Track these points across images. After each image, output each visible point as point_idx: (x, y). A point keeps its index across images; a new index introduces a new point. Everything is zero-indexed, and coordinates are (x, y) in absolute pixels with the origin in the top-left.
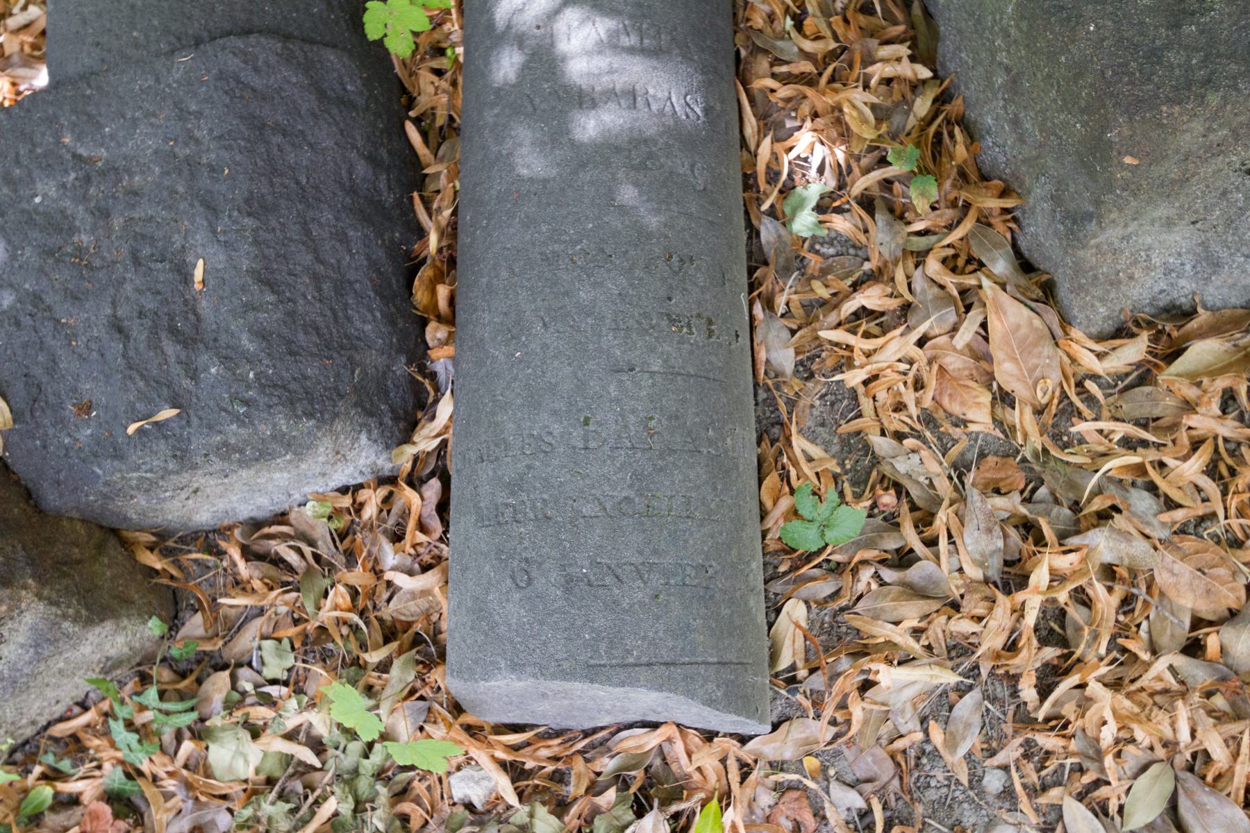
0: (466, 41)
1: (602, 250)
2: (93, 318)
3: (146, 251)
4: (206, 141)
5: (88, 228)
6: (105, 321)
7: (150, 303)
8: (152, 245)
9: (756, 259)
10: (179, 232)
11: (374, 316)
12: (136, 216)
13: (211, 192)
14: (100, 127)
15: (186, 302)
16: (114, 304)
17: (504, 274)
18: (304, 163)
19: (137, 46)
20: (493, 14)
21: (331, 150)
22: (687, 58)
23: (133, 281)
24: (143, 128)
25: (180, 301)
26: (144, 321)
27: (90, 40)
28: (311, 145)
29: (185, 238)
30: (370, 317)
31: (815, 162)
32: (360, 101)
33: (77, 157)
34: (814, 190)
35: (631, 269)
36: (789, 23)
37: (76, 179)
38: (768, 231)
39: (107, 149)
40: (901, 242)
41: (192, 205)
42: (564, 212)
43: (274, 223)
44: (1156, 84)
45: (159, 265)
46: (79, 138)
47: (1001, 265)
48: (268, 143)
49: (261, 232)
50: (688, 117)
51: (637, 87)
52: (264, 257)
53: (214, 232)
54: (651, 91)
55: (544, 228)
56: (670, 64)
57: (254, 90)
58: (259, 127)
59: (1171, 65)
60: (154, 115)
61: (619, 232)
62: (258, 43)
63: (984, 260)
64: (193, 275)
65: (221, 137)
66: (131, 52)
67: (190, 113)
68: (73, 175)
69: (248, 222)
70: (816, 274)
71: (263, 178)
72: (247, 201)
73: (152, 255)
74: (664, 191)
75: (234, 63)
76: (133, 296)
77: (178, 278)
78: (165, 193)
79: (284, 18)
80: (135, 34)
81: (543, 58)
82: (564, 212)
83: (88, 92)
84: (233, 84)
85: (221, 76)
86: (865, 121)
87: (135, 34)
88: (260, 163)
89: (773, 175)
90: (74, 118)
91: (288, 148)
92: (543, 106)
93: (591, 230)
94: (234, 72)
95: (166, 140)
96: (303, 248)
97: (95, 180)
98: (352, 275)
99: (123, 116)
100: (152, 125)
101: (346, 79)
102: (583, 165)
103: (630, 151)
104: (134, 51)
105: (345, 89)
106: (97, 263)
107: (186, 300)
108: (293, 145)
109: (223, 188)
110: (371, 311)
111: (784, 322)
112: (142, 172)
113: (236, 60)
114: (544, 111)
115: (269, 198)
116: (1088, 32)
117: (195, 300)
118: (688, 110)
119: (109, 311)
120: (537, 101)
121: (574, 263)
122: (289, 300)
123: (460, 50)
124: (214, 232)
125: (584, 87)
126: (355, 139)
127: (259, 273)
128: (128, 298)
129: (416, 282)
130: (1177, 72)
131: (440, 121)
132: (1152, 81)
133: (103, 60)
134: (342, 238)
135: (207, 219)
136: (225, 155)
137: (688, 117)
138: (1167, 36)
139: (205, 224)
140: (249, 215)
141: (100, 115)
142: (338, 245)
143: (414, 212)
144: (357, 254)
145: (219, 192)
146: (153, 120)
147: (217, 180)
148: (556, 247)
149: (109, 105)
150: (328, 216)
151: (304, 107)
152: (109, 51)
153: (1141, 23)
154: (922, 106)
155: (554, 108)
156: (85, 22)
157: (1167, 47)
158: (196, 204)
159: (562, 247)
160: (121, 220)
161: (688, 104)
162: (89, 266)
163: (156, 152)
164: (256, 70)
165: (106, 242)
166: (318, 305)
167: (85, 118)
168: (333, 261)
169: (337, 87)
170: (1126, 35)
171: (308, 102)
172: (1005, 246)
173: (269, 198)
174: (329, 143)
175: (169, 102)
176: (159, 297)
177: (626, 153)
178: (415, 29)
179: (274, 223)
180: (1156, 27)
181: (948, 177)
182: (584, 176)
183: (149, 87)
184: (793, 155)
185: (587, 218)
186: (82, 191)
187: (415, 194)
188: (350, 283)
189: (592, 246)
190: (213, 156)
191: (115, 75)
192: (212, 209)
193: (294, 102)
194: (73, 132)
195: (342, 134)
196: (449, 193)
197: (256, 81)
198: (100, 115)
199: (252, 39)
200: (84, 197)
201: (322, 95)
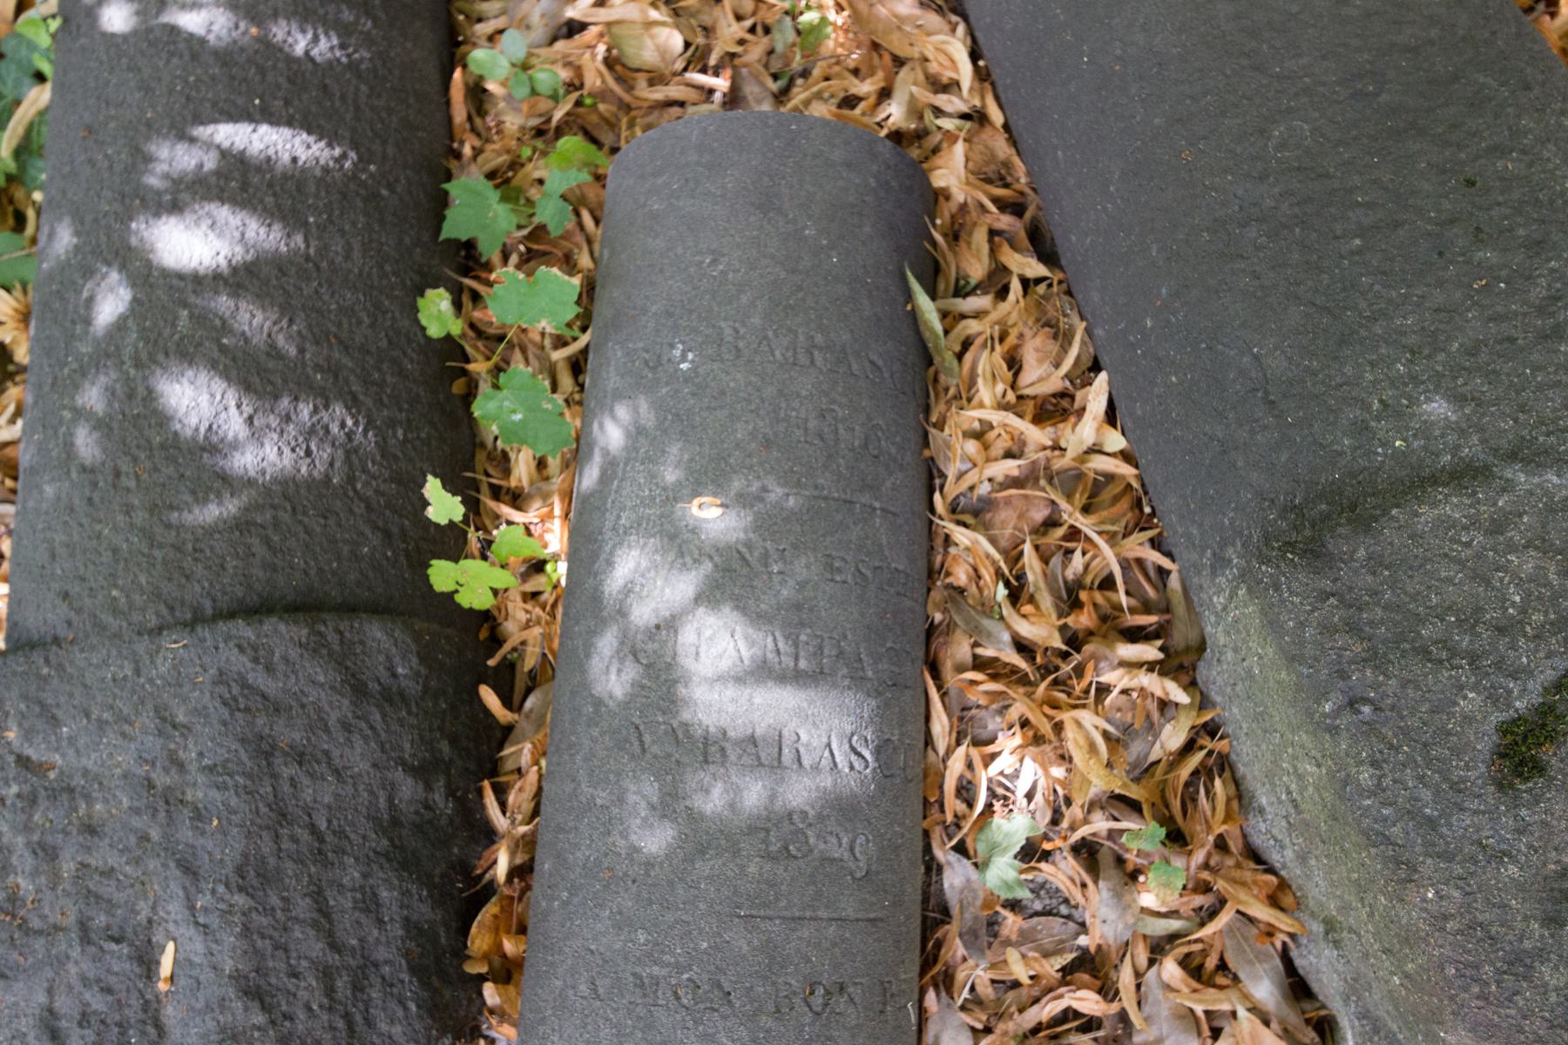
0: (574, 556)
1: (719, 986)
2: (22, 1004)
3: (101, 920)
4: (193, 768)
5: (27, 869)
6: (37, 1012)
7: (98, 1003)
8: (108, 913)
9: (935, 913)
10: (146, 899)
11: (406, 1009)
12: (93, 863)
13: (193, 847)
14: (55, 722)
15: (146, 1006)
16: (50, 992)
17: (584, 988)
18: (326, 800)
19: (115, 611)
20: (601, 583)
21: (364, 774)
22: (857, 680)
23: (79, 962)
24: (111, 737)
25: (135, 1002)
26: (87, 1032)
27: (56, 586)
28: (337, 772)
29: (154, 908)
30: (400, 1013)
31: (1022, 787)
32: (413, 688)
33: (23, 762)
34: (1014, 826)
35: (754, 1015)
36: (1002, 592)
37: (19, 796)
38: (956, 876)
39: (63, 755)
40: (1131, 921)
41: (165, 866)
42: (670, 917)
43: (275, 900)
44: (1520, 1009)
45: (114, 946)
46: (28, 735)
47: (1265, 989)
48: (275, 777)
49: (254, 915)
50: (852, 768)
51: (785, 732)
52: (256, 951)
53: (192, 908)
54: (804, 737)
55: (642, 937)
56: (834, 693)
57: (264, 696)
58: (264, 750)
59: (1545, 985)
60: (127, 721)
61: (744, 957)
62: (276, 630)
63: (1242, 975)
64: (158, 963)
65: (211, 769)
66: (107, 618)
67: (174, 727)
68: (14, 789)
69: (240, 900)
70: (1014, 937)
71: (264, 834)
72: (240, 871)
73: (108, 928)
74: (811, 890)
75: (239, 662)
76: (78, 987)
77: (138, 970)
78: (133, 840)
79: (321, 570)
80: (114, 593)
81: (660, 676)
82: (670, 917)
83: (45, 671)
84: (236, 690)
85: (221, 678)
86: (1092, 748)
87: (114, 593)
88: (264, 810)
89: (966, 791)
90: (22, 706)
91: (306, 781)
92: (655, 749)
93: (705, 952)
94: (239, 673)
95: (141, 759)
96: (312, 933)
97: (43, 803)
98: (381, 954)
99: (87, 716)
100: (124, 735)
101: (397, 659)
102: (702, 851)
103: (768, 831)
104: (111, 619)
105: (394, 675)
106: (35, 923)
107: (147, 1002)
108: (311, 775)
109: (210, 845)
110: (402, 1002)
111: (965, 1018)
112: (106, 801)
113: (244, 659)
114: (655, 757)
115: (272, 861)
116: (1424, 900)
117: (158, 1001)
118: (853, 758)
119: (42, 998)
120: (647, 739)
121: (678, 998)
122: (286, 1016)
123: (563, 567)
124: (192, 908)
125: (712, 729)
126: (403, 750)
127: (246, 978)
128: (70, 987)
129: (474, 930)
130: (1553, 998)
131: (530, 662)
132: (1515, 1004)
133: (69, 623)
134: (369, 904)
135: (185, 888)
136: (215, 794)
137: (852, 768)
138: (1542, 936)
139: (181, 893)
140: (241, 889)
141: (58, 705)
142: (363, 920)
143: (483, 807)
144: (384, 931)
145: (203, 847)
146: (126, 727)
147: (203, 833)
148: (656, 970)
149: (71, 695)
150: (352, 874)
151: (333, 718)
152: (79, 611)
153: (1504, 906)
154: (1173, 736)
155: (669, 756)
156: (53, 556)
157: (1541, 954)
158: (172, 865)
159: (664, 972)
160: (72, 866)
161: (853, 749)
162: (24, 927)
163: (125, 776)
164: (270, 669)
165: (48, 896)
166: (325, 1017)
167: (37, 709)
168: (354, 942)
169: (382, 672)
170: (1480, 918)
171: (338, 708)
172: (1272, 957)
173: (272, 861)
174: (364, 766)
175: (150, 706)
176: (110, 998)
177: (762, 835)
178: (495, 586)
179: (275, 900)
180: (1526, 918)
181: (1203, 846)
182: (703, 868)
183: (125, 678)
184: (994, 769)
185: (701, 931)
186: (24, 817)
187: (486, 783)
188: (376, 965)
189: (705, 976)
190: (200, 795)
191: (82, 651)
192: (189, 869)
193: (319, 710)
194: (20, 725)
195: (383, 751)
196: (532, 777)
197: (270, 686)
198: (58, 705)
199: (269, 624)
200: (26, 826)
201: (359, 690)
